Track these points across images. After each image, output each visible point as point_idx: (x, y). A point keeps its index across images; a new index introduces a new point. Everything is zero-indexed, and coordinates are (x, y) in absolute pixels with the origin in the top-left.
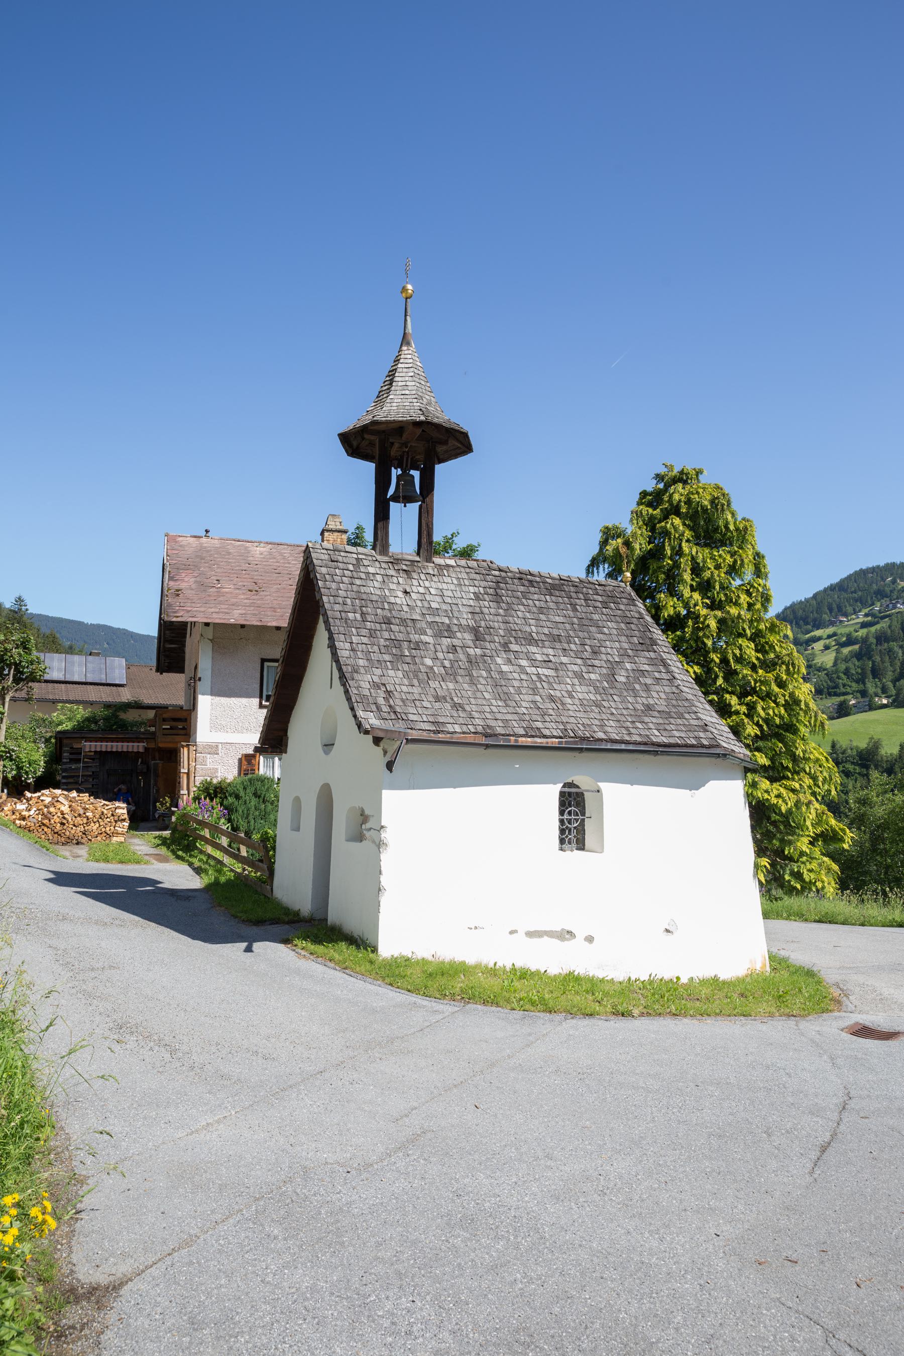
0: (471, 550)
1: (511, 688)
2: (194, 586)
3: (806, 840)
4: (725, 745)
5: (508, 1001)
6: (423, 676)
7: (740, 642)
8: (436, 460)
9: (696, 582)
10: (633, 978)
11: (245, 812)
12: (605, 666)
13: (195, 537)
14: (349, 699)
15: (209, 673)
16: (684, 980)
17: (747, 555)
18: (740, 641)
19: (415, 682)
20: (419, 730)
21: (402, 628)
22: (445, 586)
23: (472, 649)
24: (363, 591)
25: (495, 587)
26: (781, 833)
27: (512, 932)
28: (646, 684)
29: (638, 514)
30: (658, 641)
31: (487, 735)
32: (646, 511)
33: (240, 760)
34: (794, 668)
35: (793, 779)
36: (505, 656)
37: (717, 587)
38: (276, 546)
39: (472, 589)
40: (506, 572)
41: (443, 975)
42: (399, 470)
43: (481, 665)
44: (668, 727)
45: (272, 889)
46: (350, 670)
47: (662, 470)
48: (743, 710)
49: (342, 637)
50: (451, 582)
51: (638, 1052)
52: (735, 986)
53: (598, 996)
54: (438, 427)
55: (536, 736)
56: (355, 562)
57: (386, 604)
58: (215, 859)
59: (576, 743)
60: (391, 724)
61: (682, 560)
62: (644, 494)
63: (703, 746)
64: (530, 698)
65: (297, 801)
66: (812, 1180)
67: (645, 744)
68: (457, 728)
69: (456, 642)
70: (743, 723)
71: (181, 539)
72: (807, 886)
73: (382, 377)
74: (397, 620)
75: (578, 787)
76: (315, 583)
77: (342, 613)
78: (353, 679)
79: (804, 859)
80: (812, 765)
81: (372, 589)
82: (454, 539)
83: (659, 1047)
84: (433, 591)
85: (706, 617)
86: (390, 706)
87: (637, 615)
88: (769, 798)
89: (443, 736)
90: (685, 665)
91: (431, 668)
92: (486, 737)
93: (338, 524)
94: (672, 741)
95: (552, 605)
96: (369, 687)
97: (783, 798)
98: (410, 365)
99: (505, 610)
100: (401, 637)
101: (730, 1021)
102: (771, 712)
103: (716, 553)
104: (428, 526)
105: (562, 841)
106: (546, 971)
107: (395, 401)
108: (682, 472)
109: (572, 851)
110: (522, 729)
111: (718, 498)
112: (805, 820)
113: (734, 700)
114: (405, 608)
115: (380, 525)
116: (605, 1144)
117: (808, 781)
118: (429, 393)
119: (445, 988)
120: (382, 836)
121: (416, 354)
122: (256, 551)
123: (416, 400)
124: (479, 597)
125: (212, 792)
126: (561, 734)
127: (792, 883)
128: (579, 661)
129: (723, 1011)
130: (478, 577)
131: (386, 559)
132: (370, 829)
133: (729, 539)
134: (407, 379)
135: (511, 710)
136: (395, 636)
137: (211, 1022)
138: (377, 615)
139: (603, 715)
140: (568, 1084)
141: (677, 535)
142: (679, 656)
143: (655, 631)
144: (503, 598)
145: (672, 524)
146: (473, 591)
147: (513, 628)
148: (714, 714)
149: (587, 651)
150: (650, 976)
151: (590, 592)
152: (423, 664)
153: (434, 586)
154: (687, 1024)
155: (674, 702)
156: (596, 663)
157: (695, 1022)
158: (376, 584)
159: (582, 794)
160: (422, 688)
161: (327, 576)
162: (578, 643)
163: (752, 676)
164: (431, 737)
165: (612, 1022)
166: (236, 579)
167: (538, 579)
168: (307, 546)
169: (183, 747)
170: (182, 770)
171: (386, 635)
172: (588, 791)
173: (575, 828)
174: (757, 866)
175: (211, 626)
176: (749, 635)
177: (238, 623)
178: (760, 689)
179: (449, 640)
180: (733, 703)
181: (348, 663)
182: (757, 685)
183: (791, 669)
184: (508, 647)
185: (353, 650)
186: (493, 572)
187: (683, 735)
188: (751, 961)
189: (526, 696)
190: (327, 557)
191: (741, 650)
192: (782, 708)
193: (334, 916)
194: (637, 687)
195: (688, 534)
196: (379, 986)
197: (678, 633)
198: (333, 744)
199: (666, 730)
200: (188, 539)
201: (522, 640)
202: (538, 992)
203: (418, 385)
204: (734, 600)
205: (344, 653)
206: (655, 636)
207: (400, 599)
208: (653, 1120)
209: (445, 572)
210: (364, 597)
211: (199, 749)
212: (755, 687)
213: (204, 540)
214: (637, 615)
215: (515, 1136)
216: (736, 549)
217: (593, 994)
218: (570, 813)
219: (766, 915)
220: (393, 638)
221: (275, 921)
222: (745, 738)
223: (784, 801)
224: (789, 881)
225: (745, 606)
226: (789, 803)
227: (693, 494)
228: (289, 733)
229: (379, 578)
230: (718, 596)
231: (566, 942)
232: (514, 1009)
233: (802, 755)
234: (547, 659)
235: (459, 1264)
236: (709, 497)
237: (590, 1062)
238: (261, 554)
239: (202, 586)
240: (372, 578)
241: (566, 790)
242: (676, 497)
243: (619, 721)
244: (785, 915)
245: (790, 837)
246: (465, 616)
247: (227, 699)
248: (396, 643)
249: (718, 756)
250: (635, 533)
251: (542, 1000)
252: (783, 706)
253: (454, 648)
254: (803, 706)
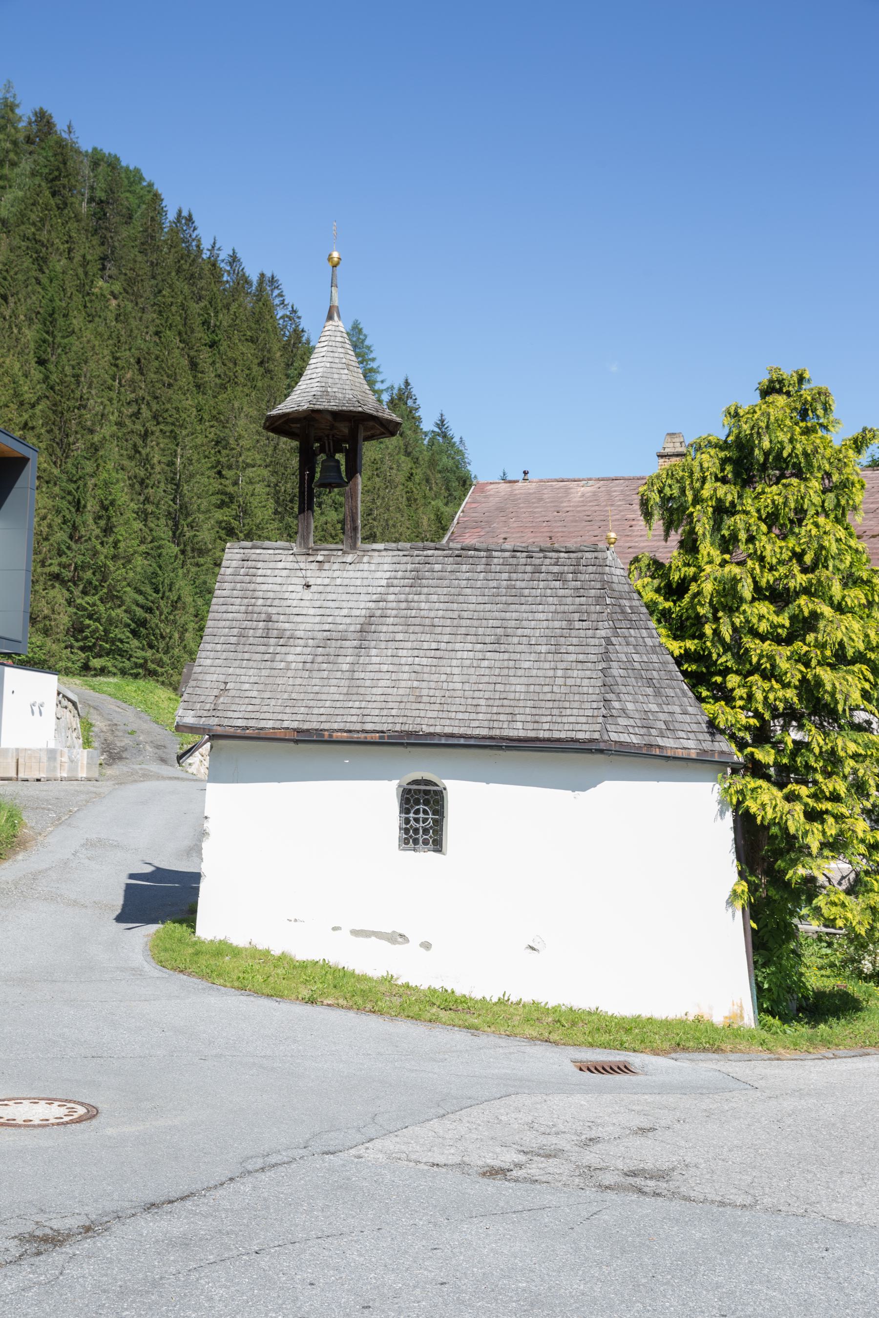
27: (335, 929)
71: (492, 486)
93: (678, 444)
219: (196, 877)
249: (601, 751)
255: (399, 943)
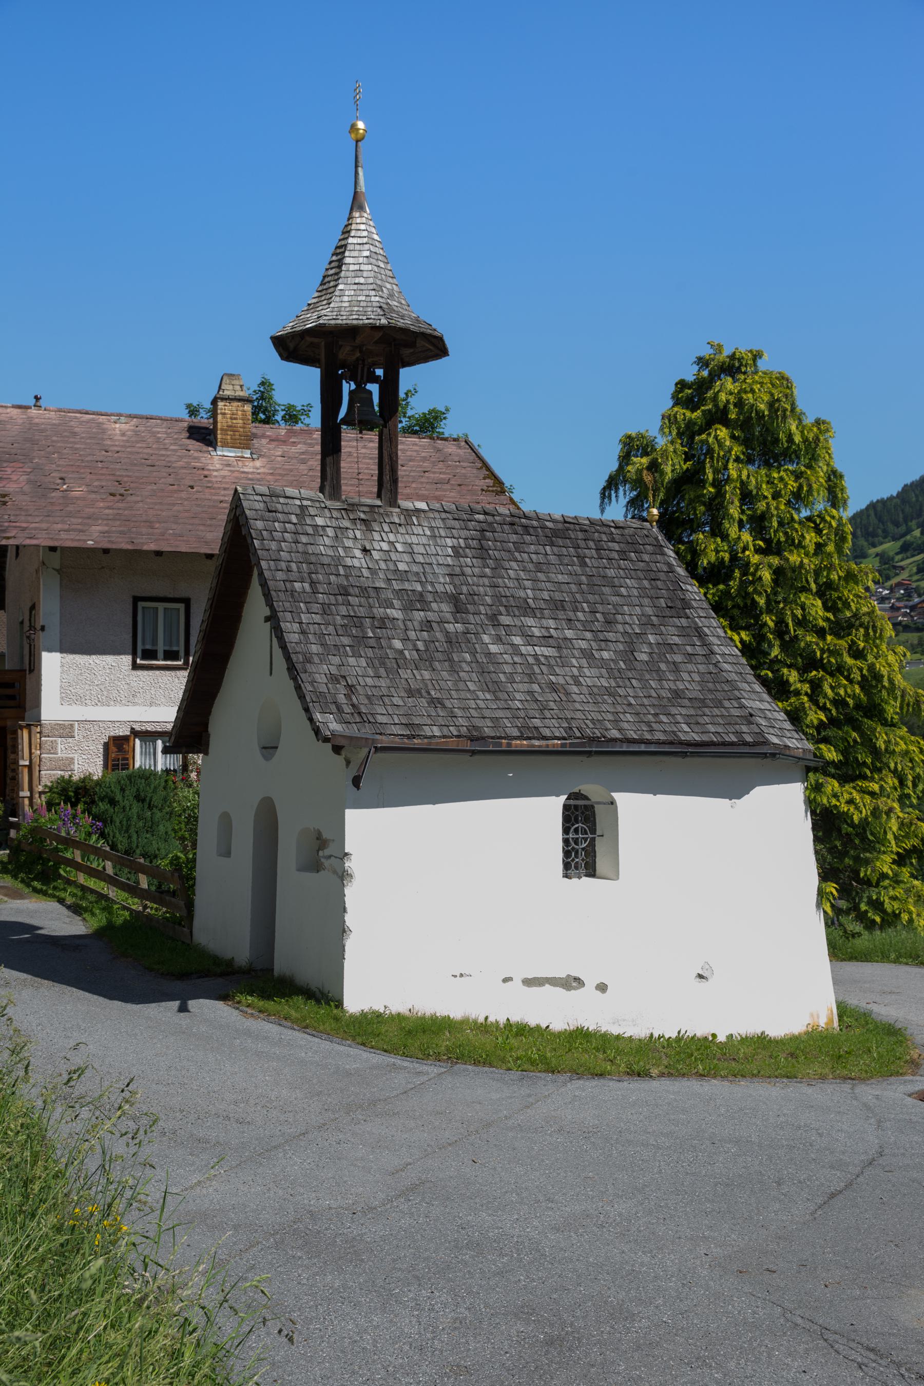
0: (436, 418)
1: (501, 675)
2: (27, 488)
3: (888, 859)
4: (775, 740)
5: (503, 1060)
6: (391, 664)
7: (803, 599)
8: (400, 365)
9: (748, 515)
10: (656, 1035)
11: (125, 823)
12: (622, 640)
13: (19, 407)
14: (302, 697)
15: (56, 619)
16: (722, 1038)
17: (817, 478)
18: (802, 598)
19: (382, 671)
20: (390, 735)
21: (362, 600)
22: (414, 539)
23: (451, 625)
24: (310, 552)
25: (479, 537)
26: (856, 849)
27: (506, 980)
28: (674, 663)
29: (669, 419)
30: (693, 602)
31: (472, 739)
32: (683, 414)
33: (106, 746)
34: (875, 632)
35: (872, 779)
36: (493, 633)
37: (775, 524)
38: (145, 421)
39: (449, 542)
40: (493, 516)
41: (424, 1032)
42: (352, 383)
43: (463, 645)
44: (701, 720)
45: (191, 932)
46: (301, 660)
47: (706, 352)
48: (804, 689)
49: (288, 616)
50: (422, 533)
51: (652, 1113)
52: (784, 1044)
53: (610, 1055)
54: (405, 331)
55: (534, 738)
56: (298, 512)
57: (340, 568)
58: (92, 891)
59: (582, 745)
60: (356, 728)
61: (727, 488)
62: (682, 385)
63: (746, 744)
64: (526, 687)
65: (226, 822)
66: (811, 1218)
67: (671, 743)
68: (436, 731)
69: (431, 616)
70: (804, 708)
72: (890, 920)
73: (326, 255)
74: (356, 589)
75: (586, 798)
76: (249, 541)
77: (287, 584)
78: (306, 672)
79: (886, 882)
80: (899, 759)
81: (322, 548)
82: (409, 399)
83: (678, 1107)
84: (400, 547)
85: (757, 566)
86: (353, 705)
87: (665, 568)
88: (838, 804)
89: (420, 741)
90: (729, 632)
91: (401, 652)
92: (472, 741)
93: (238, 388)
94: (705, 738)
95: (553, 559)
96: (326, 681)
97: (856, 804)
98: (365, 240)
99: (492, 569)
100: (362, 612)
101: (769, 1083)
102: (842, 692)
103: (775, 475)
104: (391, 458)
105: (566, 866)
106: (548, 1027)
107: (347, 293)
108: (732, 357)
109: (580, 878)
110: (516, 729)
111: (778, 400)
112: (885, 832)
113: (793, 676)
114: (366, 573)
115: (329, 460)
116: (608, 1191)
117: (892, 781)
118: (390, 280)
119: (428, 1047)
120: (346, 865)
121: (371, 223)
122: (114, 429)
123: (373, 293)
124: (458, 552)
125: (72, 794)
126: (565, 735)
127: (869, 915)
128: (588, 635)
129: (762, 1073)
130: (456, 524)
131: (338, 505)
132: (330, 857)
133: (795, 451)
134: (361, 260)
135: (501, 704)
136: (355, 612)
137: (165, 1089)
138: (330, 584)
139: (618, 706)
140: (571, 1142)
141: (722, 453)
142: (721, 620)
143: (689, 587)
144: (491, 552)
145: (716, 437)
146: (450, 544)
147: (503, 594)
148: (766, 697)
149: (598, 621)
150: (679, 1032)
151: (604, 538)
152: (391, 647)
153: (400, 541)
154: (715, 1085)
155: (710, 685)
156: (611, 636)
157: (726, 1083)
158: (327, 541)
159: (593, 807)
160: (391, 679)
161: (264, 533)
162: (587, 610)
163: (817, 644)
164: (404, 743)
165: (625, 1083)
166: (89, 476)
167: (535, 523)
168: (236, 490)
169: (21, 728)
170: (22, 763)
171: (343, 610)
172: (599, 803)
173: (583, 849)
174: (821, 893)
175: (59, 551)
176: (814, 590)
177: (99, 546)
178: (829, 661)
179: (422, 613)
180: (791, 680)
181: (298, 649)
182: (825, 656)
183: (872, 634)
184: (498, 620)
185: (303, 632)
186: (477, 516)
187: (720, 730)
188: (812, 1015)
189: (520, 685)
190: (262, 505)
191: (803, 609)
192: (857, 686)
193: (280, 966)
194: (663, 666)
195: (737, 450)
196: (350, 1046)
197: (721, 587)
198: (277, 748)
199: (698, 723)
200: (9, 410)
201: (515, 609)
202: (539, 1050)
203: (376, 269)
204: (797, 541)
205: (292, 637)
206: (689, 596)
207: (358, 560)
208: (660, 1172)
209: (414, 519)
210: (313, 559)
211: (45, 731)
212: (822, 659)
213: (34, 412)
214: (665, 568)
215: (516, 1184)
216: (803, 468)
217: (604, 1052)
218: (576, 831)
220: (352, 614)
221: (205, 974)
222: (808, 726)
223: (857, 808)
224: (866, 912)
225: (811, 549)
226: (864, 811)
227: (746, 392)
228: (211, 729)
229: (330, 531)
230: (775, 535)
231: (573, 991)
232: (510, 1069)
233: (883, 747)
234: (547, 635)
235: (469, 1271)
236: (766, 398)
237: (597, 1122)
238: (123, 435)
239: (40, 489)
240: (322, 533)
241: (572, 802)
242: (723, 397)
243: (638, 714)
244: (893, 956)
245: (868, 855)
246: (442, 580)
247: (85, 656)
248: (355, 620)
249: (765, 756)
250: (666, 450)
251: (543, 1059)
252: (859, 683)
253: (428, 624)
254: (886, 684)
255: (575, 988)
